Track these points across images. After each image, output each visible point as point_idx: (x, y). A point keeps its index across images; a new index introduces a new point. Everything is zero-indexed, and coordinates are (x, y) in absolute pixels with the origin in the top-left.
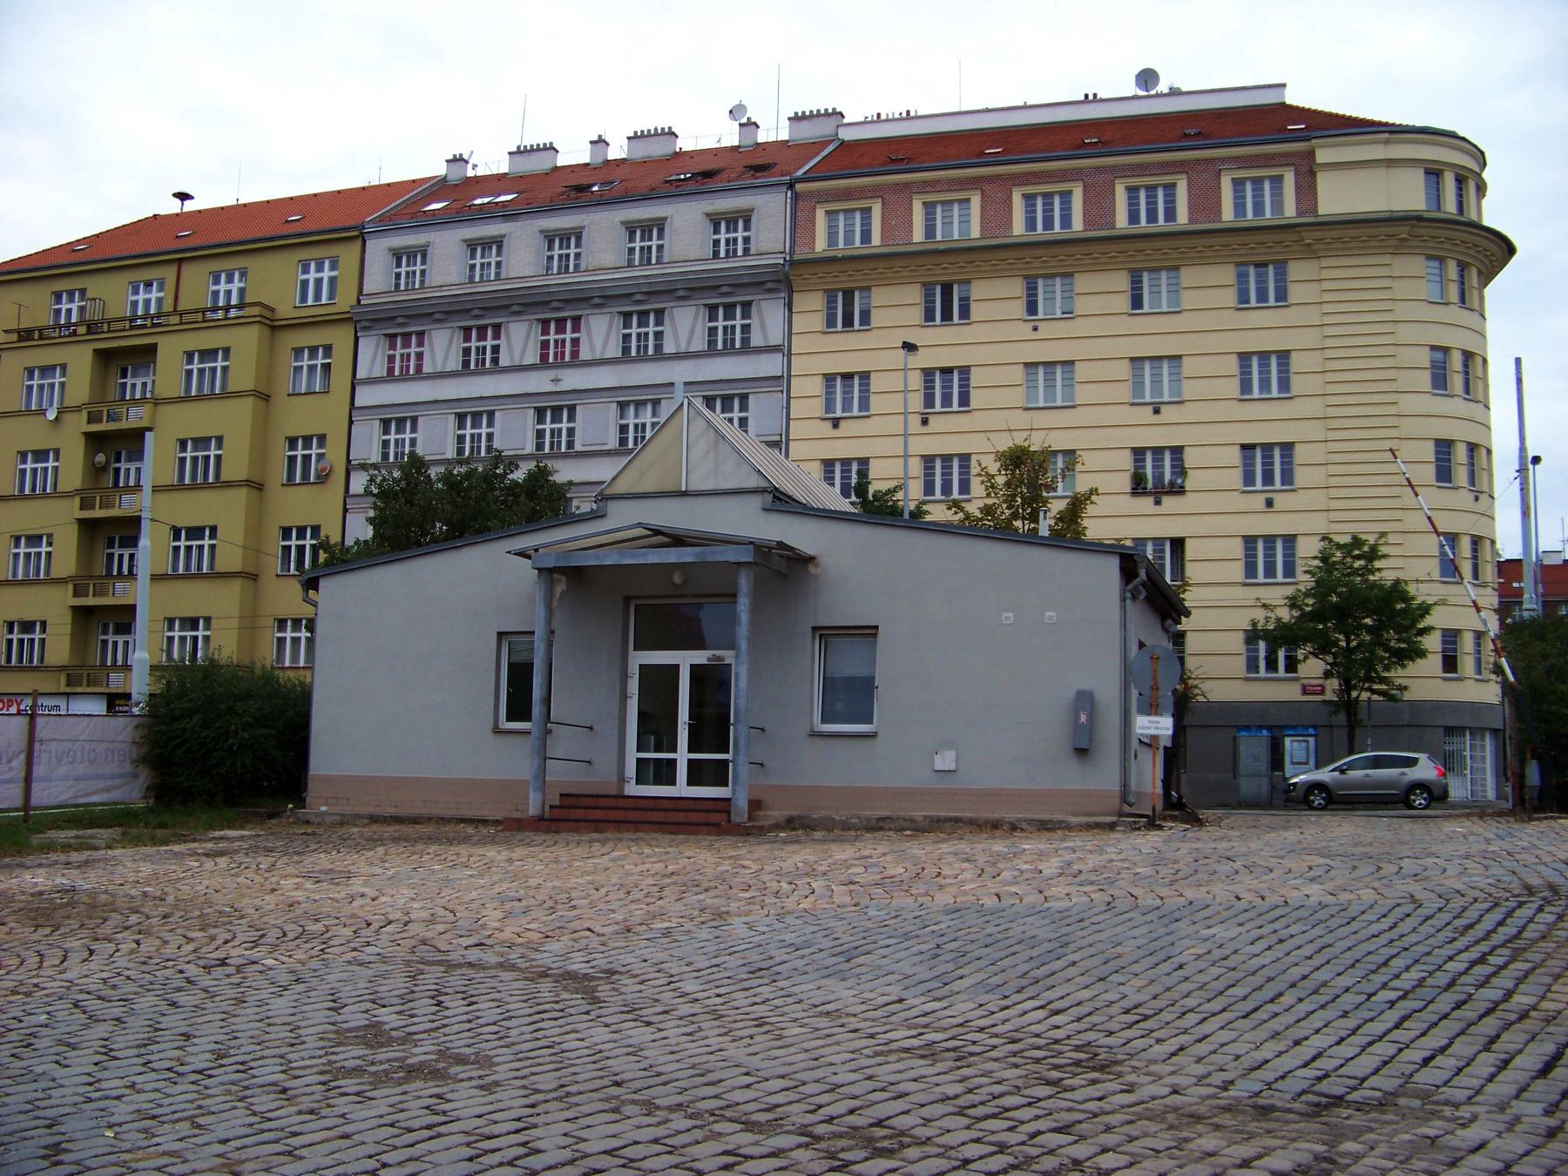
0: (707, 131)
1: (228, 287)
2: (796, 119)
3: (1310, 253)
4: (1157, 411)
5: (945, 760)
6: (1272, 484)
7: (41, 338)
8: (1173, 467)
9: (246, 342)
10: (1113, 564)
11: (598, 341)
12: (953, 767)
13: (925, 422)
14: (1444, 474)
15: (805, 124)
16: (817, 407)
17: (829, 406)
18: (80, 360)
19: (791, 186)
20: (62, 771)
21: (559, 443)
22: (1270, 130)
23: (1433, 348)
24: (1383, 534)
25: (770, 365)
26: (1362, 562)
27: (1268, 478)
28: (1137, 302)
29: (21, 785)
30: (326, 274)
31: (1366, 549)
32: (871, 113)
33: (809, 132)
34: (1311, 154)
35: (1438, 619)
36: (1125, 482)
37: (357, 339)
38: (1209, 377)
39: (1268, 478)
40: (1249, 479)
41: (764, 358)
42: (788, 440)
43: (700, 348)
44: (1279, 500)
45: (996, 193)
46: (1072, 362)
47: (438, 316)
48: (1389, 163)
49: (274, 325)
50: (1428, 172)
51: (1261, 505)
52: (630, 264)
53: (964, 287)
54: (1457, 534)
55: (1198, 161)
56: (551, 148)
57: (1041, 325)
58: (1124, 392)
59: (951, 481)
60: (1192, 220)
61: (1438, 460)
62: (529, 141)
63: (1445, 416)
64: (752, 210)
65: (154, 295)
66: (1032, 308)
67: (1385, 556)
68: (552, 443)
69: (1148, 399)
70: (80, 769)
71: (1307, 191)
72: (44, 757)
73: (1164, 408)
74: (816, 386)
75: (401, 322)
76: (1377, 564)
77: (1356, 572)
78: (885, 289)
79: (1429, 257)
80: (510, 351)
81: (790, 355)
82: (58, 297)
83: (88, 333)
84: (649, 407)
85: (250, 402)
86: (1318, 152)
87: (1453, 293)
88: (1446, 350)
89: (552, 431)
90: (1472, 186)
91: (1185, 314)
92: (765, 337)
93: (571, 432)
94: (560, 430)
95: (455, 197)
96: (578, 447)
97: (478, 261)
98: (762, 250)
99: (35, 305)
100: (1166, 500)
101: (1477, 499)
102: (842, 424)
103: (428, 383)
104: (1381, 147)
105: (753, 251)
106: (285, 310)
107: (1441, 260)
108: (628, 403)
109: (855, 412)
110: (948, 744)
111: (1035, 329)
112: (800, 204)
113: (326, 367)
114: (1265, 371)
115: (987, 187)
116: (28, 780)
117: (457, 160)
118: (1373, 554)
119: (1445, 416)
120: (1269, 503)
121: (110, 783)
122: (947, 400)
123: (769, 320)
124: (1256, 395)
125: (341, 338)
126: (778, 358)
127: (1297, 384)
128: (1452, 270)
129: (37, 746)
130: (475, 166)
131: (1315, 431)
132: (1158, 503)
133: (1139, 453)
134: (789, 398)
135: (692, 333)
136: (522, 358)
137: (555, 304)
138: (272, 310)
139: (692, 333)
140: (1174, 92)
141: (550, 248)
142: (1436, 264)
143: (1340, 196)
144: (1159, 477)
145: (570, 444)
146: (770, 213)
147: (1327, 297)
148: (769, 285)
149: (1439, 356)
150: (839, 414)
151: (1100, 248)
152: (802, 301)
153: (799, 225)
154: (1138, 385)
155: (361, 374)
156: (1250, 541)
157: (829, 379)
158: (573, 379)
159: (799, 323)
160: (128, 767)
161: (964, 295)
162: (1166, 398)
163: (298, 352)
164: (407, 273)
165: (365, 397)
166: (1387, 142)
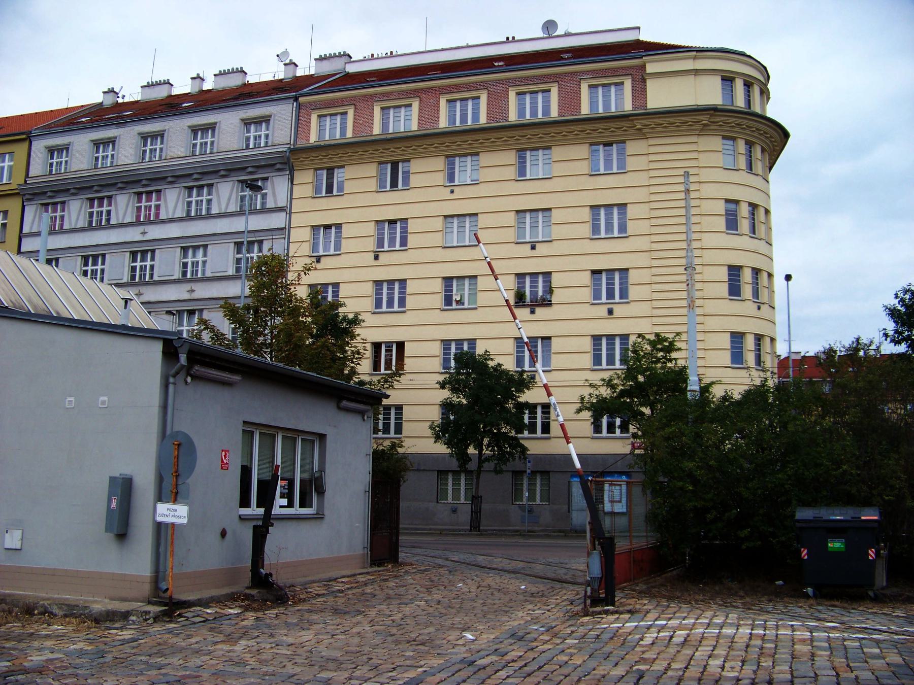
0: (264, 69)
2: (321, 59)
3: (641, 135)
4: (533, 248)
5: (13, 540)
6: (613, 298)
8: (544, 286)
10: (158, 347)
11: (171, 205)
12: (18, 547)
13: (376, 258)
14: (735, 290)
15: (325, 62)
17: (315, 247)
19: (296, 99)
21: (145, 275)
22: (627, 55)
23: (728, 201)
24: (678, 334)
25: (277, 221)
26: (662, 354)
27: (610, 295)
28: (522, 172)
31: (666, 344)
32: (368, 54)
33: (327, 68)
34: (643, 67)
38: (570, 222)
39: (610, 295)
40: (597, 295)
41: (274, 216)
44: (618, 310)
45: (429, 99)
46: (476, 214)
47: (72, 191)
48: (696, 72)
50: (724, 79)
53: (406, 164)
54: (763, 336)
55: (566, 74)
56: (168, 83)
57: (455, 189)
58: (511, 235)
60: (560, 114)
61: (730, 280)
62: (157, 78)
63: (739, 249)
64: (270, 116)
66: (451, 177)
67: (680, 349)
68: (140, 275)
69: (528, 240)
71: (640, 92)
73: (538, 245)
74: (306, 234)
76: (674, 355)
77: (658, 360)
78: (356, 167)
79: (724, 138)
80: (117, 213)
81: (291, 213)
84: (201, 250)
86: (647, 65)
87: (742, 163)
88: (737, 202)
89: (141, 267)
90: (756, 90)
91: (554, 179)
92: (275, 202)
93: (152, 267)
94: (146, 266)
95: (108, 114)
96: (156, 278)
97: (101, 154)
98: (276, 142)
101: (759, 308)
102: (322, 259)
103: (66, 236)
104: (691, 61)
105: (270, 144)
107: (734, 139)
108: (188, 247)
109: (332, 252)
110: (18, 524)
111: (452, 192)
112: (302, 112)
114: (608, 217)
115: (423, 96)
117: (111, 91)
118: (671, 348)
119: (739, 249)
120: (610, 312)
122: (392, 242)
123: (277, 189)
124: (603, 235)
127: (631, 227)
128: (741, 146)
130: (123, 97)
131: (642, 260)
132: (533, 312)
133: (520, 276)
134: (289, 242)
135: (229, 199)
136: (174, 213)
137: (144, 182)
139: (229, 199)
140: (568, 35)
141: (145, 145)
142: (731, 142)
143: (660, 96)
144: (534, 293)
145: (151, 276)
146: (282, 113)
147: (653, 166)
148: (278, 166)
149: (732, 206)
150: (321, 253)
151: (497, 134)
152: (299, 177)
153: (300, 125)
154: (521, 227)
155: (26, 230)
156: (597, 339)
157: (315, 228)
158: (155, 232)
159: (298, 191)
161: (406, 169)
162: (540, 239)
164: (57, 163)
166: (695, 58)
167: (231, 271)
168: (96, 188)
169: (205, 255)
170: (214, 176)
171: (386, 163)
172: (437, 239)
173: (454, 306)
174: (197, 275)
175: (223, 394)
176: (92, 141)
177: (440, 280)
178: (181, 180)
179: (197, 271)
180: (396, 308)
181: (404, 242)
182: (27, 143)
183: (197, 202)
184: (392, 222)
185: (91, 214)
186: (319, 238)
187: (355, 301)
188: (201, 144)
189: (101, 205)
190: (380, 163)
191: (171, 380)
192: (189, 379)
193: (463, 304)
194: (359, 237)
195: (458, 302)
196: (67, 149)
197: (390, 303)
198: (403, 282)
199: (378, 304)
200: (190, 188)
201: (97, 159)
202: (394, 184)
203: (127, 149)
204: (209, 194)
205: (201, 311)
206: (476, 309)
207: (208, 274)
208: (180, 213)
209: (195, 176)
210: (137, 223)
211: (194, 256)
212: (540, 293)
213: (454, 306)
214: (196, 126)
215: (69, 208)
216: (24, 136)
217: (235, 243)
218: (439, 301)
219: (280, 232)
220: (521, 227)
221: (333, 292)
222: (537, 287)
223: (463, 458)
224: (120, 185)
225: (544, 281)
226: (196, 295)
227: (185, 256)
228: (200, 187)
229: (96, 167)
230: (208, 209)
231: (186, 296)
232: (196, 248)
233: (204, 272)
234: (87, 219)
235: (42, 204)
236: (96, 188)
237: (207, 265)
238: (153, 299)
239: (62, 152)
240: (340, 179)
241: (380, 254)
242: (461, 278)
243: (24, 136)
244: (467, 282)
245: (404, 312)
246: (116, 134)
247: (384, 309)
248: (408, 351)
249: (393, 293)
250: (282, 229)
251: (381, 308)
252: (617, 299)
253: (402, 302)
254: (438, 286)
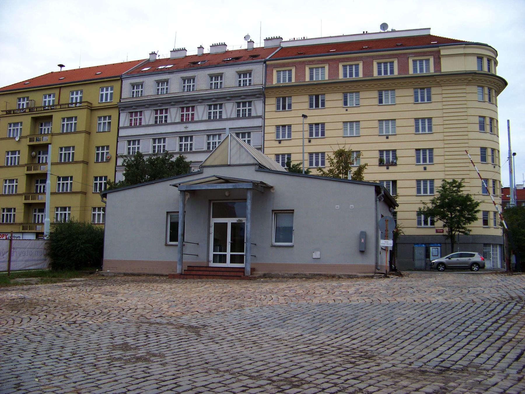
0: (237, 44)
1: (76, 96)
2: (267, 40)
3: (439, 85)
4: (387, 138)
5: (317, 255)
6: (426, 162)
7: (14, 113)
8: (393, 156)
9: (82, 115)
10: (373, 189)
11: (200, 114)
12: (319, 257)
13: (310, 141)
14: (484, 159)
15: (269, 41)
16: (274, 136)
17: (278, 136)
18: (27, 120)
19: (265, 62)
20: (21, 258)
21: (187, 148)
22: (425, 44)
23: (480, 117)
24: (463, 179)
25: (258, 122)
26: (456, 188)
27: (425, 160)
28: (381, 101)
29: (7, 263)
30: (109, 92)
31: (457, 184)
32: (292, 38)
33: (271, 44)
34: (439, 52)
35: (482, 207)
36: (377, 161)
37: (119, 114)
38: (405, 126)
39: (425, 160)
40: (418, 160)
41: (256, 120)
42: (264, 147)
43: (234, 117)
44: (428, 167)
45: (333, 65)
46: (359, 121)
47: (147, 106)
48: (465, 55)
49: (92, 109)
50: (478, 58)
51: (422, 169)
52: (211, 89)
53: (323, 96)
54: (488, 179)
55: (401, 54)
56: (184, 50)
57: (348, 109)
58: (376, 131)
59: (318, 161)
60: (399, 74)
61: (481, 154)
62: (177, 47)
63: (484, 139)
64: (252, 70)
65: (52, 99)
66: (345, 103)
67: (464, 186)
68: (185, 149)
69: (384, 134)
70: (27, 258)
71: (438, 64)
72: (15, 253)
73: (390, 137)
74: (273, 129)
75: (134, 108)
76: (461, 189)
77: (454, 192)
78: (296, 97)
79: (479, 86)
80: (171, 118)
81: (264, 119)
82: (19, 99)
83: (30, 112)
84: (217, 136)
85: (84, 135)
86: (441, 51)
87: (487, 98)
88: (484, 117)
89: (185, 144)
90: (493, 62)
91: (397, 105)
92: (256, 113)
93: (191, 145)
94: (187, 144)
95: (152, 66)
96: (194, 150)
97: (160, 87)
98: (255, 84)
99: (12, 102)
100: (390, 167)
101: (494, 167)
102: (282, 142)
103: (143, 128)
104: (462, 49)
105: (252, 84)
106: (96, 104)
107: (483, 87)
108: (210, 135)
109: (286, 138)
110: (318, 249)
111: (347, 110)
112: (268, 68)
113: (109, 123)
114: (424, 124)
115: (330, 63)
116: (9, 261)
117: (153, 54)
118: (460, 186)
119: (484, 139)
120: (425, 169)
121: (37, 262)
122: (317, 134)
123: (257, 107)
124: (420, 132)
125: (114, 113)
126: (260, 120)
127: (434, 129)
128: (486, 90)
129: (12, 250)
130: (159, 56)
131: (440, 144)
132: (388, 168)
133: (381, 152)
134: (264, 133)
135: (232, 111)
136: (175, 120)
137: (186, 102)
138: (91, 104)
139: (232, 111)
140: (393, 31)
141: (184, 83)
142: (481, 88)
143: (449, 66)
144: (388, 160)
145: (191, 149)
147: (444, 99)
148: (258, 96)
149: (482, 119)
150: (281, 139)
151: (368, 83)
152: (269, 101)
153: (267, 75)
154: (381, 129)
155: (121, 125)
156: (418, 181)
157: (278, 127)
158: (192, 127)
159: (267, 108)
160: (43, 257)
161: (323, 99)
162: (390, 133)
163: (100, 118)
164: (136, 92)
165: (122, 133)
166: (464, 48)
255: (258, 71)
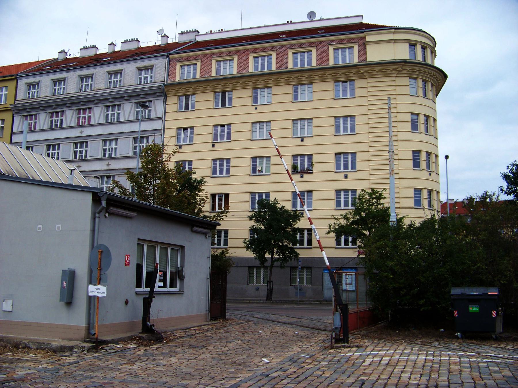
0: (150, 39)
2: (182, 33)
3: (363, 76)
4: (302, 140)
5: (7, 306)
6: (348, 169)
8: (308, 162)
10: (90, 196)
11: (97, 116)
12: (10, 310)
13: (213, 146)
14: (416, 164)
15: (184, 35)
17: (178, 140)
19: (168, 56)
21: (82, 156)
22: (355, 31)
23: (412, 114)
24: (384, 189)
25: (157, 125)
26: (375, 200)
27: (346, 167)
28: (296, 97)
31: (378, 195)
32: (208, 31)
33: (186, 38)
34: (365, 38)
38: (323, 126)
39: (346, 167)
40: (338, 167)
41: (156, 122)
44: (350, 175)
45: (243, 56)
46: (270, 121)
47: (41, 108)
48: (395, 41)
50: (410, 45)
53: (230, 93)
54: (432, 190)
55: (321, 42)
56: (95, 47)
57: (258, 107)
58: (289, 133)
60: (317, 65)
61: (414, 159)
62: (89, 44)
63: (419, 141)
64: (153, 66)
66: (256, 101)
67: (385, 198)
68: (80, 156)
69: (299, 136)
71: (363, 52)
73: (305, 139)
74: (174, 133)
76: (382, 201)
77: (373, 204)
78: (202, 94)
79: (411, 78)
80: (66, 121)
81: (165, 121)
84: (114, 142)
86: (367, 37)
87: (421, 92)
88: (417, 114)
89: (80, 151)
90: (428, 51)
91: (314, 101)
92: (156, 114)
93: (86, 151)
94: (83, 151)
95: (61, 65)
96: (88, 157)
97: (57, 87)
98: (156, 81)
101: (430, 175)
102: (183, 147)
103: (37, 134)
104: (392, 35)
105: (153, 81)
107: (416, 79)
108: (107, 140)
109: (188, 143)
110: (10, 297)
111: (256, 109)
112: (171, 63)
114: (345, 123)
115: (240, 54)
117: (63, 52)
118: (380, 197)
119: (419, 141)
120: (346, 177)
122: (222, 137)
123: (157, 107)
124: (342, 133)
127: (358, 129)
128: (420, 83)
130: (70, 55)
131: (364, 147)
132: (302, 177)
133: (295, 157)
134: (164, 137)
135: (130, 113)
136: (99, 120)
137: (82, 103)
139: (130, 113)
140: (322, 20)
141: (82, 82)
142: (414, 81)
143: (374, 54)
144: (303, 166)
145: (86, 156)
147: (370, 94)
148: (158, 94)
149: (415, 117)
150: (182, 143)
151: (282, 76)
152: (170, 100)
153: (170, 71)
154: (295, 129)
155: (15, 130)
156: (338, 192)
157: (179, 129)
158: (88, 131)
159: (169, 108)
161: (230, 96)
162: (306, 135)
164: (32, 92)
166: (394, 33)
167: (131, 154)
168: (54, 107)
169: (116, 144)
170: (121, 100)
171: (219, 92)
172: (248, 136)
173: (257, 173)
174: (111, 156)
175: (127, 223)
176: (52, 80)
177: (249, 159)
178: (103, 102)
179: (112, 153)
180: (224, 174)
181: (229, 137)
182: (15, 81)
183: (112, 114)
184: (222, 126)
185: (52, 121)
186: (181, 135)
187: (201, 170)
188: (114, 81)
189: (57, 116)
190: (215, 92)
191: (97, 215)
192: (107, 215)
193: (262, 172)
194: (203, 134)
195: (259, 171)
196: (38, 84)
197: (221, 172)
198: (228, 160)
199: (214, 172)
200: (108, 107)
201: (55, 90)
202: (223, 104)
203: (72, 84)
204: (119, 110)
205: (114, 176)
206: (270, 175)
207: (118, 155)
208: (102, 121)
209: (111, 100)
210: (78, 126)
211: (110, 145)
212: (306, 166)
213: (257, 173)
214: (111, 71)
215: (39, 118)
216: (14, 77)
217: (133, 137)
218: (249, 170)
219: (159, 132)
220: (295, 129)
221: (189, 165)
222: (304, 162)
223: (263, 259)
224: (68, 105)
225: (308, 159)
226: (111, 167)
227: (105, 145)
228: (114, 106)
229: (54, 95)
230: (118, 119)
231: (106, 168)
232: (111, 140)
233: (115, 154)
234: (50, 124)
235: (24, 116)
236: (54, 107)
237: (118, 150)
238: (87, 169)
239: (35, 86)
240: (193, 102)
241: (215, 144)
242: (261, 158)
243: (14, 77)
244: (264, 160)
245: (229, 177)
246: (66, 76)
247: (218, 175)
248: (231, 199)
249: (223, 166)
250: (160, 130)
251: (216, 174)
252: (350, 169)
253: (228, 171)
254: (248, 162)
255: (160, 64)
